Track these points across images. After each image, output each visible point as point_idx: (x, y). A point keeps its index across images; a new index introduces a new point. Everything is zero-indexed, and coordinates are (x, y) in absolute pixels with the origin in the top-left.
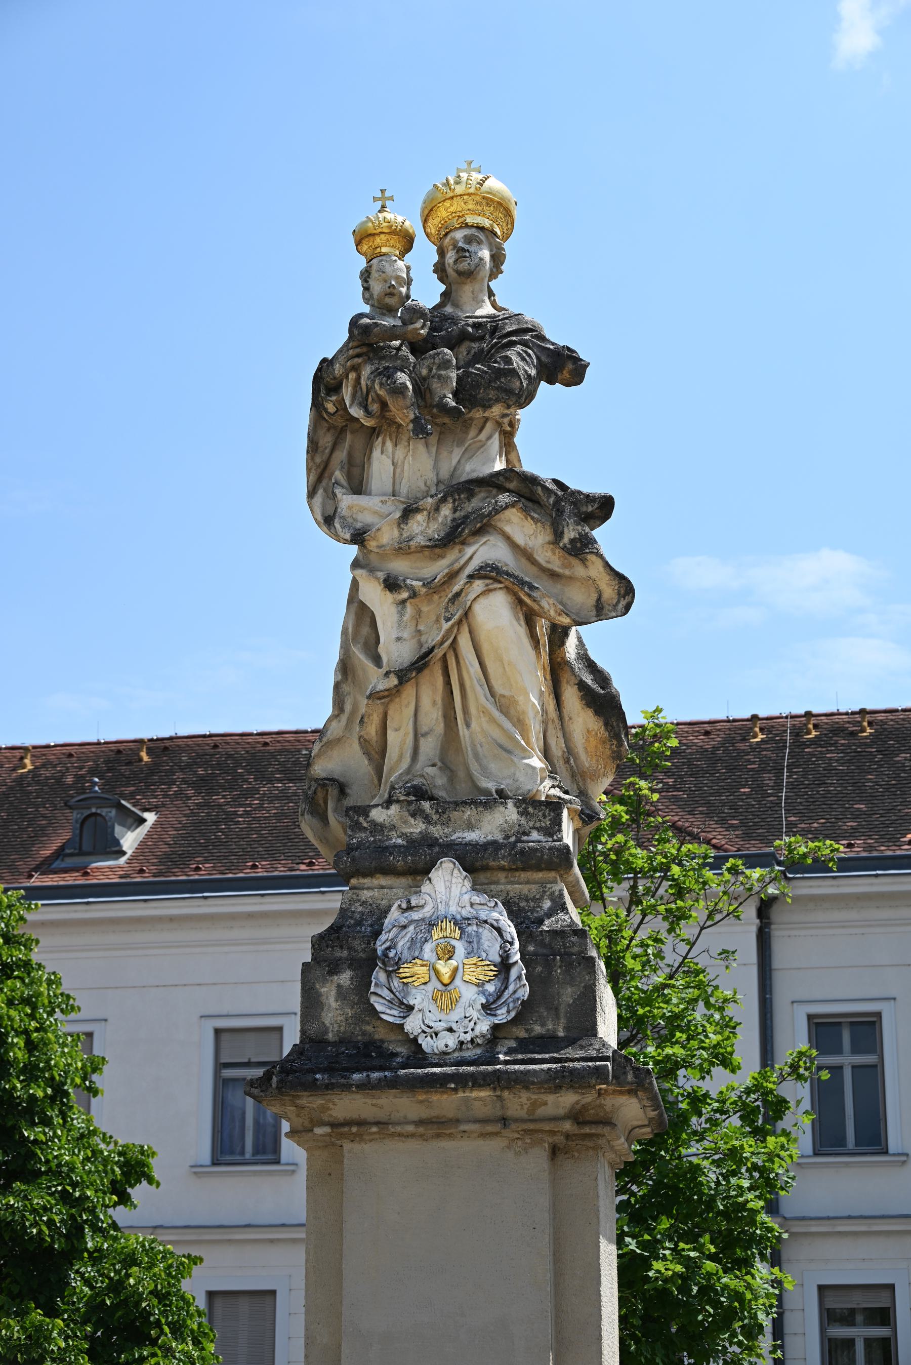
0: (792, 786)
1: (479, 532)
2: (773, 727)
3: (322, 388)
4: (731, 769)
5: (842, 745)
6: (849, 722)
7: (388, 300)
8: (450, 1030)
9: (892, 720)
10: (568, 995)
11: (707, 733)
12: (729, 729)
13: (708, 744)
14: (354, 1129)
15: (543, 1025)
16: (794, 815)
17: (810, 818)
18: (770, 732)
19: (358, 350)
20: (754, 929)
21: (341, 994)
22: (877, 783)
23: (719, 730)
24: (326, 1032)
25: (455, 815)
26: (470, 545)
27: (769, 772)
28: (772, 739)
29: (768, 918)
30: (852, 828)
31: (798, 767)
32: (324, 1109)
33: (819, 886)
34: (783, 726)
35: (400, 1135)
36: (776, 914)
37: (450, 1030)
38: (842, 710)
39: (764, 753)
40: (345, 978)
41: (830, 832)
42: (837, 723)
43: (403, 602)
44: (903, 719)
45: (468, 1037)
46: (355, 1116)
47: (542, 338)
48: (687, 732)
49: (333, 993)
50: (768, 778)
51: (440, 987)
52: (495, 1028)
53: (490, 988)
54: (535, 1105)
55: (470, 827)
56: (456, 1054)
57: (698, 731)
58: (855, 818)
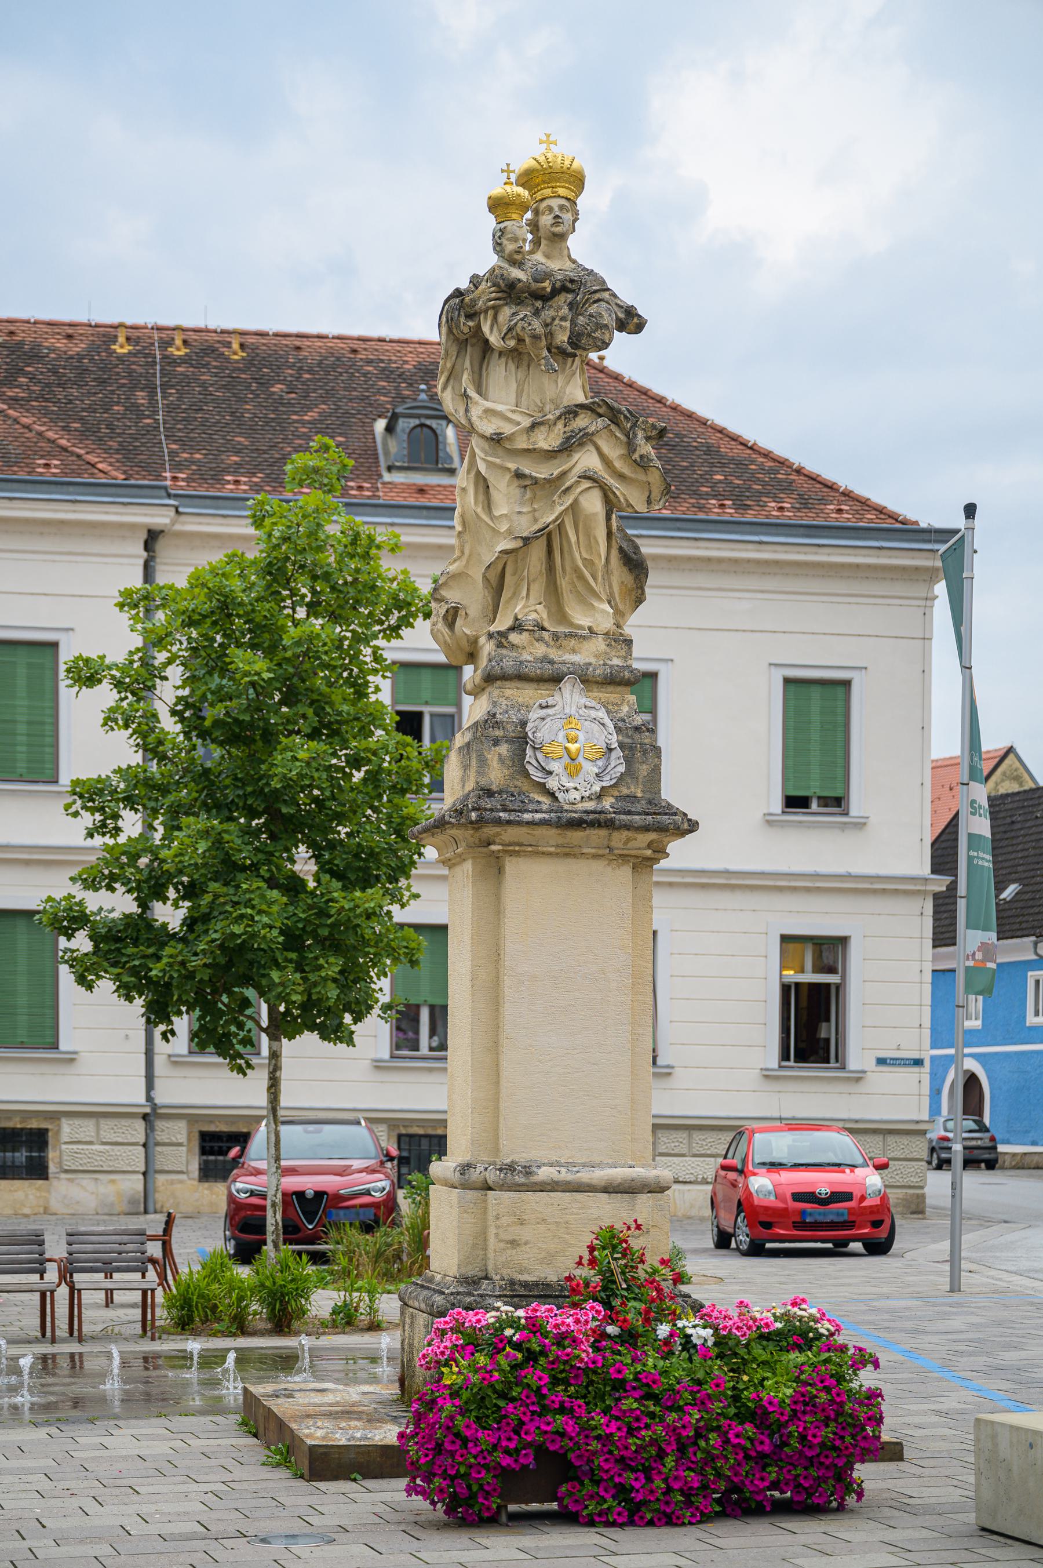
0: (169, 409)
1: (581, 444)
2: (139, 337)
3: (462, 314)
4: (102, 382)
5: (215, 367)
6: (219, 342)
7: (516, 257)
8: (576, 789)
9: (264, 344)
10: (644, 770)
11: (69, 337)
12: (93, 335)
13: (78, 348)
14: (517, 848)
15: (629, 788)
16: (175, 442)
17: (192, 447)
18: (137, 343)
19: (499, 295)
20: (141, 562)
21: (501, 760)
22: (255, 416)
23: (81, 335)
24: (491, 785)
25: (564, 643)
26: (576, 452)
27: (142, 389)
28: (139, 352)
29: (154, 552)
30: (236, 463)
31: (172, 387)
32: (498, 834)
33: (208, 524)
34: (150, 337)
35: (543, 853)
36: (160, 545)
37: (576, 789)
38: (211, 327)
39: (133, 367)
40: (504, 749)
41: (214, 465)
42: (207, 341)
43: (525, 487)
44: (275, 345)
45: (587, 794)
46: (516, 840)
47: (615, 296)
48: (47, 333)
49: (496, 758)
50: (141, 397)
51: (569, 760)
52: (603, 788)
53: (600, 763)
54: (628, 840)
55: (574, 651)
56: (580, 805)
57: (59, 334)
58: (237, 452)
